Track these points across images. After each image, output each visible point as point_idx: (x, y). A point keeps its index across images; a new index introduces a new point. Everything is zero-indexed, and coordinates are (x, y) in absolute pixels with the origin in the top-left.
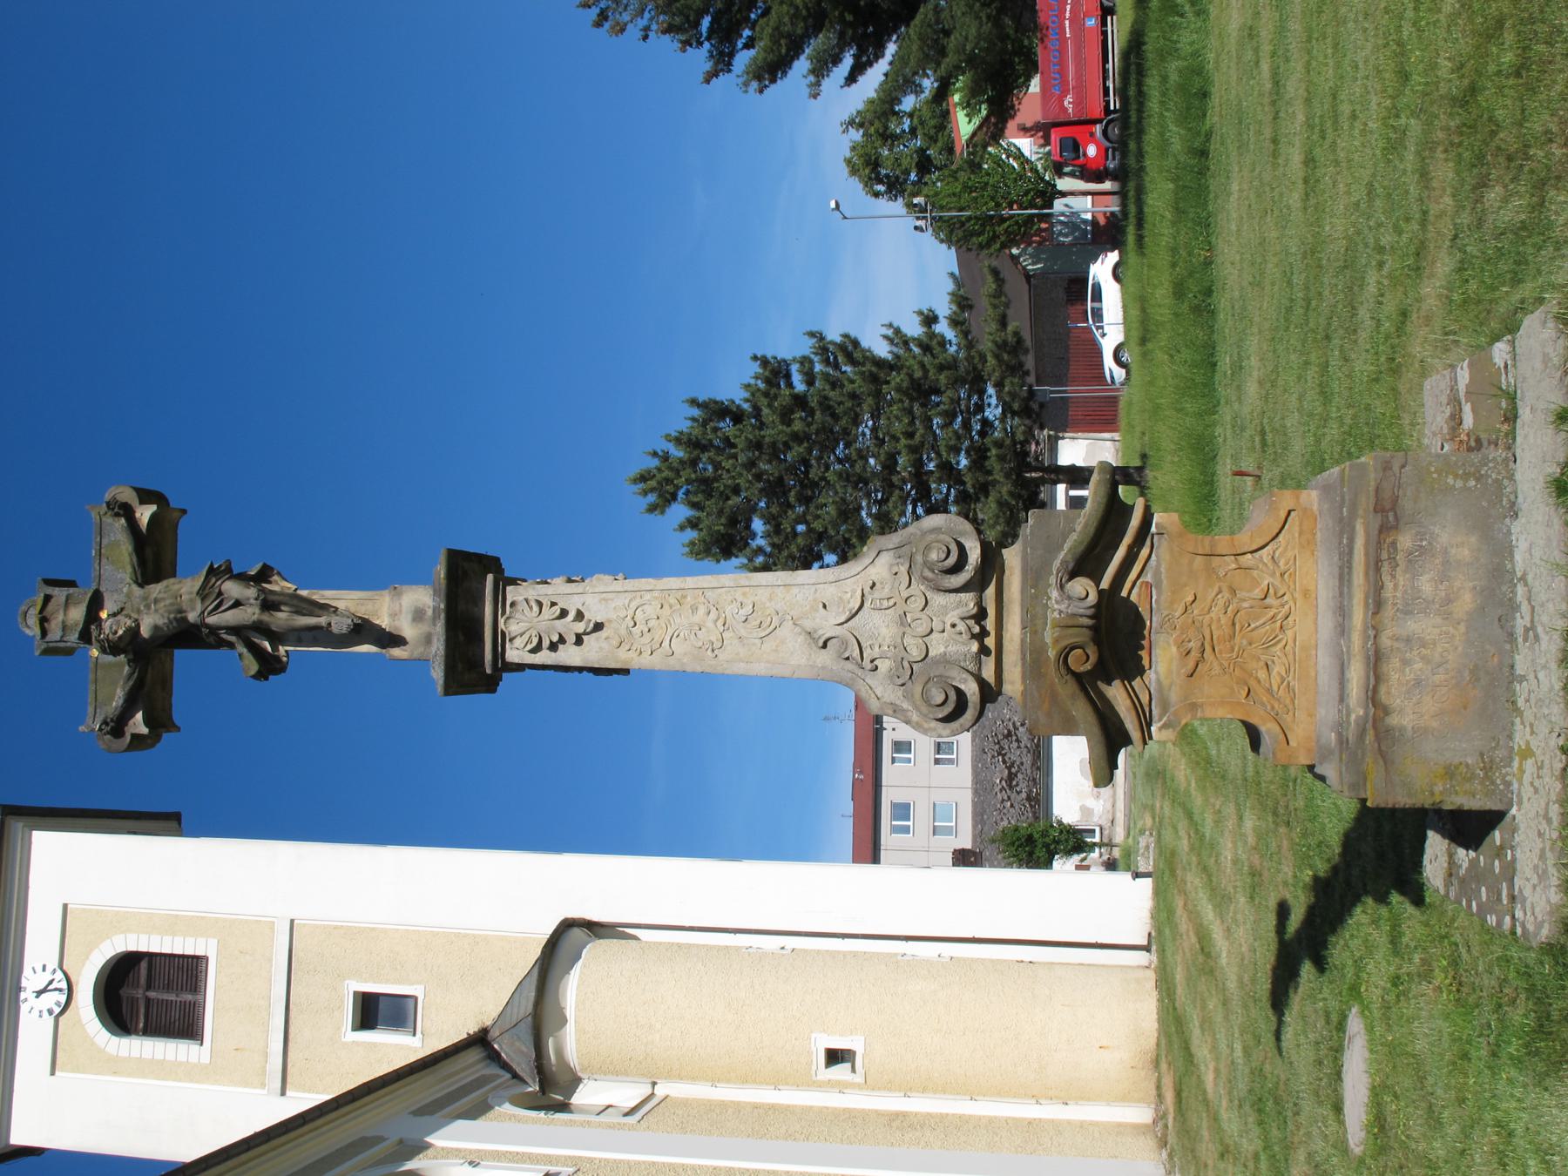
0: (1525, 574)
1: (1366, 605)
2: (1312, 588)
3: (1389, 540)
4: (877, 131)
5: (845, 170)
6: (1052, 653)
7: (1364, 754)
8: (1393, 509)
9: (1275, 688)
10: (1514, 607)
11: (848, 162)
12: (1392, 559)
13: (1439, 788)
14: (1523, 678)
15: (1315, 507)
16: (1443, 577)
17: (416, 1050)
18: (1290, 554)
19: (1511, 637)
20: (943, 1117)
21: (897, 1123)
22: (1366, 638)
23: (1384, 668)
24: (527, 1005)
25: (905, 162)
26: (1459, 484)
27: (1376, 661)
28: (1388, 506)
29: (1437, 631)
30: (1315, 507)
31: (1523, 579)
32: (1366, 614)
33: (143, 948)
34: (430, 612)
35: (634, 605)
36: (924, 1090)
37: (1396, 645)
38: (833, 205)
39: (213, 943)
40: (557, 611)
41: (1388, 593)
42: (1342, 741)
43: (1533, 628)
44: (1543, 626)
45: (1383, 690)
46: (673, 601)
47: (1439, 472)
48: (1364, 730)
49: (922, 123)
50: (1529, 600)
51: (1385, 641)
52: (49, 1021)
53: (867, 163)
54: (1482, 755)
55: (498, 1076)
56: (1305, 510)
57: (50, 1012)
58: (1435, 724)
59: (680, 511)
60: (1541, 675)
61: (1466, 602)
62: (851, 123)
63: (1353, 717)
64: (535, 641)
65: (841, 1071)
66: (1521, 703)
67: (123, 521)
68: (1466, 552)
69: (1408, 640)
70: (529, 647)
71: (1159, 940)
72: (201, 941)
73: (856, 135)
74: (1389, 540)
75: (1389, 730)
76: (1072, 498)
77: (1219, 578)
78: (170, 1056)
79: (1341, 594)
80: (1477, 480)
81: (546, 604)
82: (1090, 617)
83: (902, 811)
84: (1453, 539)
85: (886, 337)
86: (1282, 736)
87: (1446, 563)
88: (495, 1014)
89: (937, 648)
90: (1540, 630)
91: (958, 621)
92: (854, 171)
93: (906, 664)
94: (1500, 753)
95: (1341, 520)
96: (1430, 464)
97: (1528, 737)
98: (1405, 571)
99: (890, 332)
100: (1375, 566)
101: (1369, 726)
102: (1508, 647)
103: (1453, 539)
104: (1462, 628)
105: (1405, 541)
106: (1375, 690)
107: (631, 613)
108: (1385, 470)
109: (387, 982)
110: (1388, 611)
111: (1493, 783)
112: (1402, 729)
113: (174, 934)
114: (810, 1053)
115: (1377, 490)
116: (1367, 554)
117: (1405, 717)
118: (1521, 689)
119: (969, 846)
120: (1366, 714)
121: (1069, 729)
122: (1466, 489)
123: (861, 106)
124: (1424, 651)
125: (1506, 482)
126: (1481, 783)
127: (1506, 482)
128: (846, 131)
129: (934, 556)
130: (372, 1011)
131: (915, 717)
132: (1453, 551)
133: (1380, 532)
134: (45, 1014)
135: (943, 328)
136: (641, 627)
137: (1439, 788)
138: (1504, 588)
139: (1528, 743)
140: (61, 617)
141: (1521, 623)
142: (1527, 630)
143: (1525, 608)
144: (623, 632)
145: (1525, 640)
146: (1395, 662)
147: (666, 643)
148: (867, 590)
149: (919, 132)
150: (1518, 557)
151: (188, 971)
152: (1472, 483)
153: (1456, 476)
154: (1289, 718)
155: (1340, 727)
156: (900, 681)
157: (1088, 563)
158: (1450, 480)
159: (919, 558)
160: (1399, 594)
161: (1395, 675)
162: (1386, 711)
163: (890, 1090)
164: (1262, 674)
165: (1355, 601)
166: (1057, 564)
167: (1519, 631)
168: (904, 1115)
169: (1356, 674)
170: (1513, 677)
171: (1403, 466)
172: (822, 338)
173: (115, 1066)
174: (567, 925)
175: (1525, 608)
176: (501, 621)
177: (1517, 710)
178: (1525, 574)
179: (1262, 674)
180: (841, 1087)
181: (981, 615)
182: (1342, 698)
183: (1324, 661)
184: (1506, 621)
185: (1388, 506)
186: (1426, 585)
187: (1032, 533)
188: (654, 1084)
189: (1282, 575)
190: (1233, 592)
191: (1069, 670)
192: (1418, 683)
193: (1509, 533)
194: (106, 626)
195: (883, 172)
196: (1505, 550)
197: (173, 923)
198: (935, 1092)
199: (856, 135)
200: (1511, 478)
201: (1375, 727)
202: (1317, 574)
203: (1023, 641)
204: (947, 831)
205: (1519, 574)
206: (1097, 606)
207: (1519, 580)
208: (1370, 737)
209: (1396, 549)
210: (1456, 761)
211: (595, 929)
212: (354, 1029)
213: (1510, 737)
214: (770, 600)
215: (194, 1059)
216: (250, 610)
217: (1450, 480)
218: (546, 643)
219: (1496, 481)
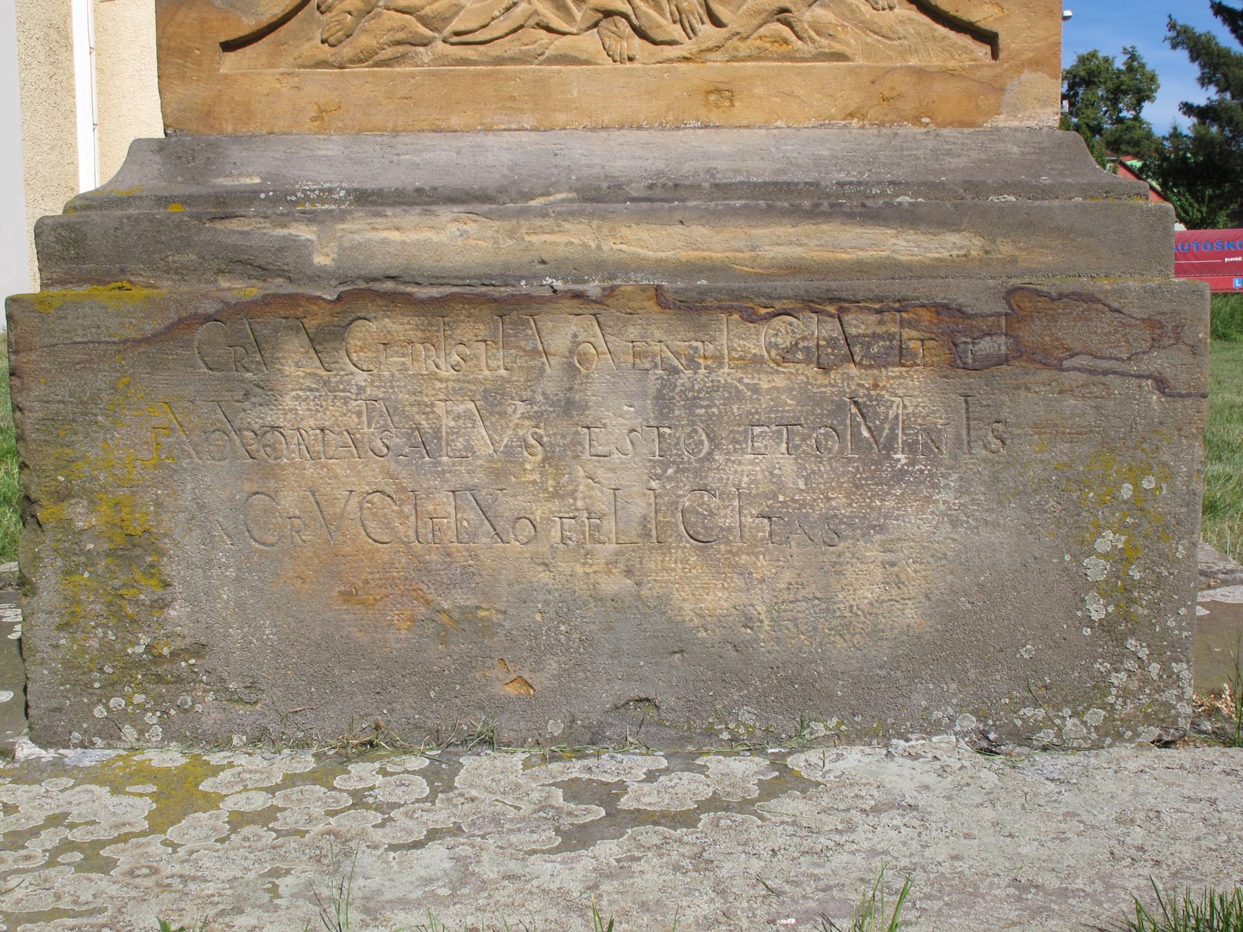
0: (804, 786)
1: (692, 269)
2: (741, 111)
4: (1122, 84)
5: (1084, 52)
7: (181, 272)
8: (1020, 352)
10: (686, 744)
11: (1094, 55)
12: (849, 349)
13: (81, 516)
14: (440, 779)
15: (1003, 121)
16: (781, 518)
18: (850, 41)
19: (586, 739)
20: (71, 91)
21: (55, 36)
22: (576, 270)
23: (470, 329)
25: (1089, 112)
26: (1096, 569)
27: (497, 302)
28: (1031, 334)
29: (603, 502)
30: (1003, 121)
31: (784, 781)
32: (658, 267)
36: (100, 70)
37: (553, 368)
38: (1067, 13)
41: (733, 338)
42: (226, 205)
43: (620, 820)
44: (622, 869)
45: (398, 325)
47: (1138, 505)
48: (265, 272)
49: (1129, 129)
50: (713, 804)
51: (563, 332)
53: (1091, 73)
54: (198, 650)
58: (289, 500)
60: (436, 857)
61: (701, 595)
62: (1133, 57)
63: (304, 232)
66: (362, 773)
68: (868, 594)
69: (569, 406)
73: (1120, 63)
75: (262, 348)
79: (722, 189)
80: (1106, 627)
84: (911, 554)
86: (248, 25)
87: (834, 530)
90: (608, 850)
92: (1083, 60)
94: (208, 708)
95: (975, 188)
96: (1169, 475)
97: (228, 805)
98: (805, 395)
100: (822, 294)
101: (278, 285)
102: (555, 727)
103: (911, 554)
104: (613, 584)
105: (910, 394)
106: (393, 300)
108: (1152, 323)
110: (665, 338)
111: (112, 686)
112: (267, 392)
115: (1088, 298)
116: (861, 269)
117: (303, 396)
118: (398, 778)
120: (318, 276)
122: (1080, 587)
123: (1149, 68)
124: (531, 462)
125: (1096, 716)
126: (108, 651)
127: (1096, 716)
128: (1125, 51)
132: (873, 552)
133: (941, 309)
137: (81, 516)
138: (747, 715)
139: (211, 801)
141: (633, 770)
142: (608, 795)
143: (686, 788)
145: (574, 790)
146: (491, 364)
149: (1120, 126)
150: (855, 759)
152: (1097, 610)
153: (1121, 559)
154: (312, 47)
155: (282, 200)
158: (1107, 541)
160: (725, 374)
161: (441, 371)
162: (326, 340)
163: (96, 30)
165: (700, 232)
167: (604, 767)
168: (68, 45)
169: (451, 241)
170: (450, 745)
171: (1161, 384)
175: (686, 788)
177: (344, 760)
178: (804, 786)
182: (370, 200)
183: (498, 151)
184: (640, 720)
185: (1031, 334)
186: (762, 465)
192: (425, 443)
193: (931, 729)
195: (1081, 91)
196: (875, 714)
198: (98, 82)
199: (1120, 63)
200: (1113, 732)
201: (267, 301)
202: (787, 122)
205: (796, 762)
207: (778, 763)
209: (880, 362)
210: (171, 569)
213: (259, 738)
217: (1107, 541)
219: (1102, 686)
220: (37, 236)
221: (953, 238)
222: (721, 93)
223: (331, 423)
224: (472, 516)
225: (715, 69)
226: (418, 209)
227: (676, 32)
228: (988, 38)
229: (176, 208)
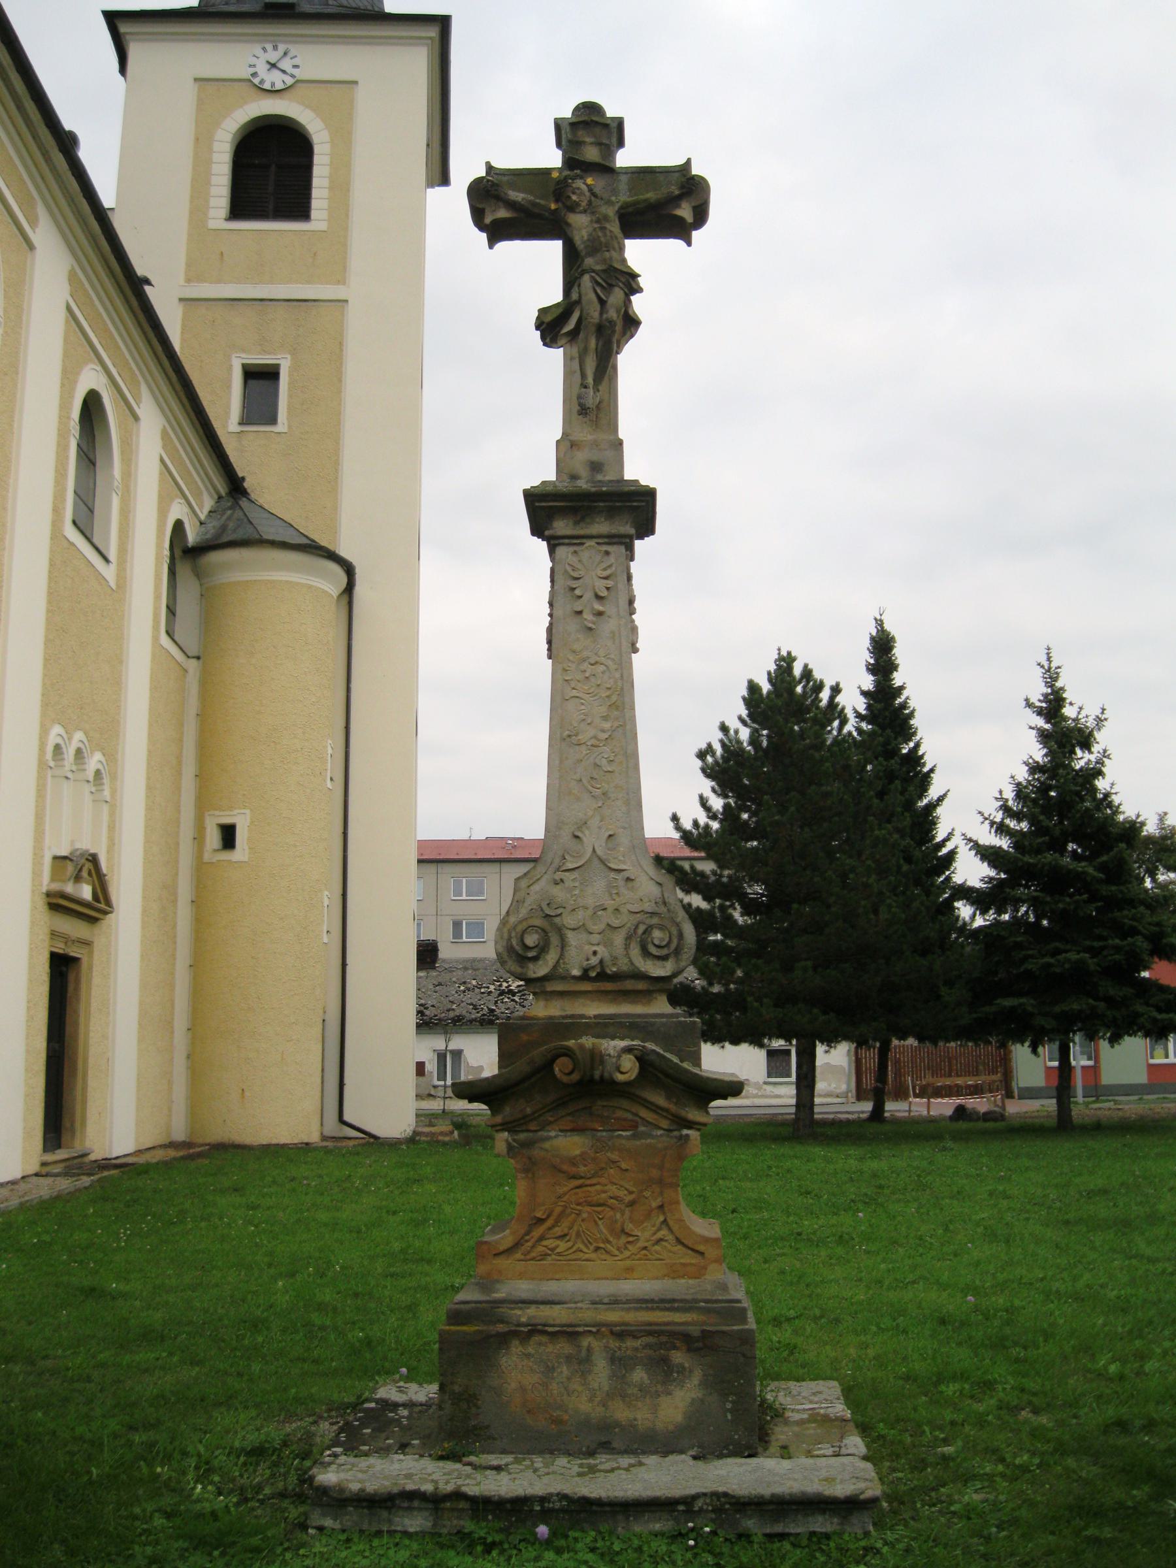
3: (678, 1343)
6: (571, 1043)
9: (545, 1243)
17: (225, 426)
19: (591, 1454)
24: (269, 533)
27: (570, 1333)
31: (641, 1464)
33: (317, 159)
34: (599, 477)
35: (610, 663)
39: (323, 226)
40: (604, 593)
45: (544, 1339)
46: (614, 698)
52: (245, 73)
55: (201, 508)
56: (705, 1268)
57: (255, 75)
64: (575, 575)
65: (213, 838)
67: (677, 192)
70: (569, 569)
71: (813, 1096)
72: (324, 215)
74: (678, 1343)
77: (641, 1191)
78: (214, 191)
81: (610, 583)
82: (602, 1076)
88: (261, 501)
91: (599, 956)
93: (559, 911)
107: (603, 660)
109: (290, 396)
113: (331, 189)
114: (231, 808)
119: (441, 955)
121: (505, 1057)
129: (657, 934)
130: (261, 378)
131: (513, 920)
134: (252, 70)
136: (590, 670)
140: (588, 140)
144: (585, 654)
147: (575, 693)
148: (626, 874)
151: (292, 202)
154: (518, 1255)
156: (545, 907)
159: (655, 921)
164: (558, 1231)
166: (650, 1046)
171: (744, 1355)
174: (349, 569)
176: (592, 543)
179: (558, 1231)
180: (199, 838)
187: (680, 1022)
188: (198, 658)
189: (645, 1248)
190: (632, 1204)
191: (558, 1056)
194: (579, 184)
197: (341, 188)
203: (582, 1016)
204: (457, 932)
206: (613, 1082)
208: (501, 1328)
212: (244, 366)
214: (616, 787)
215: (212, 213)
216: (596, 315)
218: (574, 584)
221: (688, 1315)
222: (630, 1270)
224: (562, 1390)
225: (628, 1263)
226: (347, 1494)
227: (617, 1253)
228: (702, 1254)
229: (630, 1343)
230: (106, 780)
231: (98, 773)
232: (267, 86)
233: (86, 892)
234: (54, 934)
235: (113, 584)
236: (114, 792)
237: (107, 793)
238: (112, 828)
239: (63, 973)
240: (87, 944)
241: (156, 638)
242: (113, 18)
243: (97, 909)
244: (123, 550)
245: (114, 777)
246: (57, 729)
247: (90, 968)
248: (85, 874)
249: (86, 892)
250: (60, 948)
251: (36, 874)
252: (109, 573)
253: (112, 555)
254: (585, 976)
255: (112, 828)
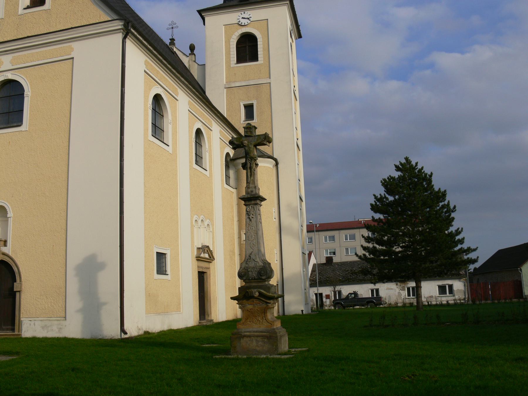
27: (249, 336)
57: (239, 21)
59: (397, 174)
61: (258, 349)
76: (445, 286)
83: (332, 238)
85: (458, 229)
89: (250, 273)
99: (460, 230)
100: (262, 336)
105: (266, 340)
110: (256, 338)
135: (459, 247)
151: (254, 57)
155: (241, 332)
157: (261, 294)
169: (248, 334)
172: (453, 212)
173: (228, 42)
174: (276, 160)
181: (255, 279)
182: (245, 332)
183: (251, 329)
186: (260, 343)
211: (277, 164)
220: (21, 111)
223: (244, 341)
230: (211, 226)
231: (208, 225)
232: (243, 24)
233: (207, 256)
234: (198, 267)
235: (208, 176)
236: (213, 229)
237: (211, 229)
238: (213, 238)
239: (202, 277)
240: (209, 268)
241: (223, 186)
242: (200, 12)
243: (211, 258)
244: (211, 166)
245: (213, 225)
246: (196, 216)
247: (210, 275)
248: (206, 251)
249: (207, 256)
250: (201, 270)
251: (192, 252)
252: (207, 173)
253: (208, 169)
254: (252, 279)
255: (213, 238)
